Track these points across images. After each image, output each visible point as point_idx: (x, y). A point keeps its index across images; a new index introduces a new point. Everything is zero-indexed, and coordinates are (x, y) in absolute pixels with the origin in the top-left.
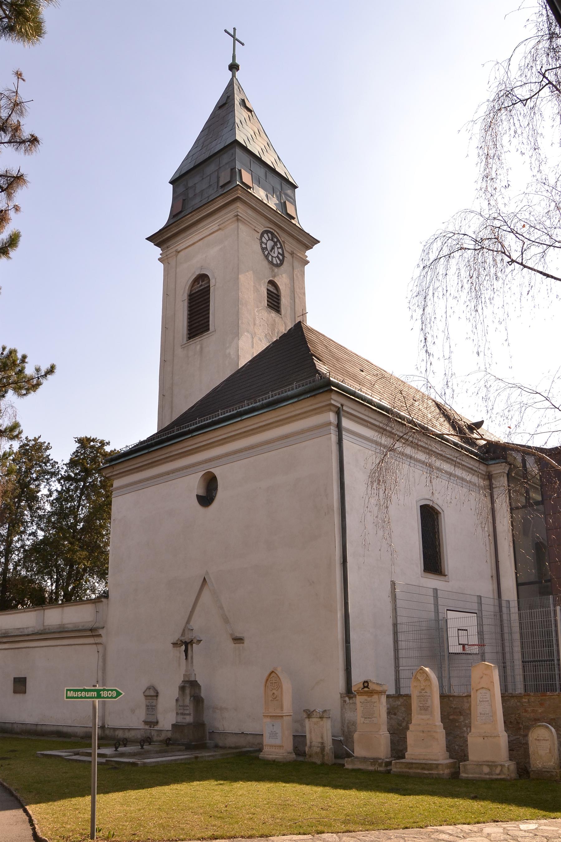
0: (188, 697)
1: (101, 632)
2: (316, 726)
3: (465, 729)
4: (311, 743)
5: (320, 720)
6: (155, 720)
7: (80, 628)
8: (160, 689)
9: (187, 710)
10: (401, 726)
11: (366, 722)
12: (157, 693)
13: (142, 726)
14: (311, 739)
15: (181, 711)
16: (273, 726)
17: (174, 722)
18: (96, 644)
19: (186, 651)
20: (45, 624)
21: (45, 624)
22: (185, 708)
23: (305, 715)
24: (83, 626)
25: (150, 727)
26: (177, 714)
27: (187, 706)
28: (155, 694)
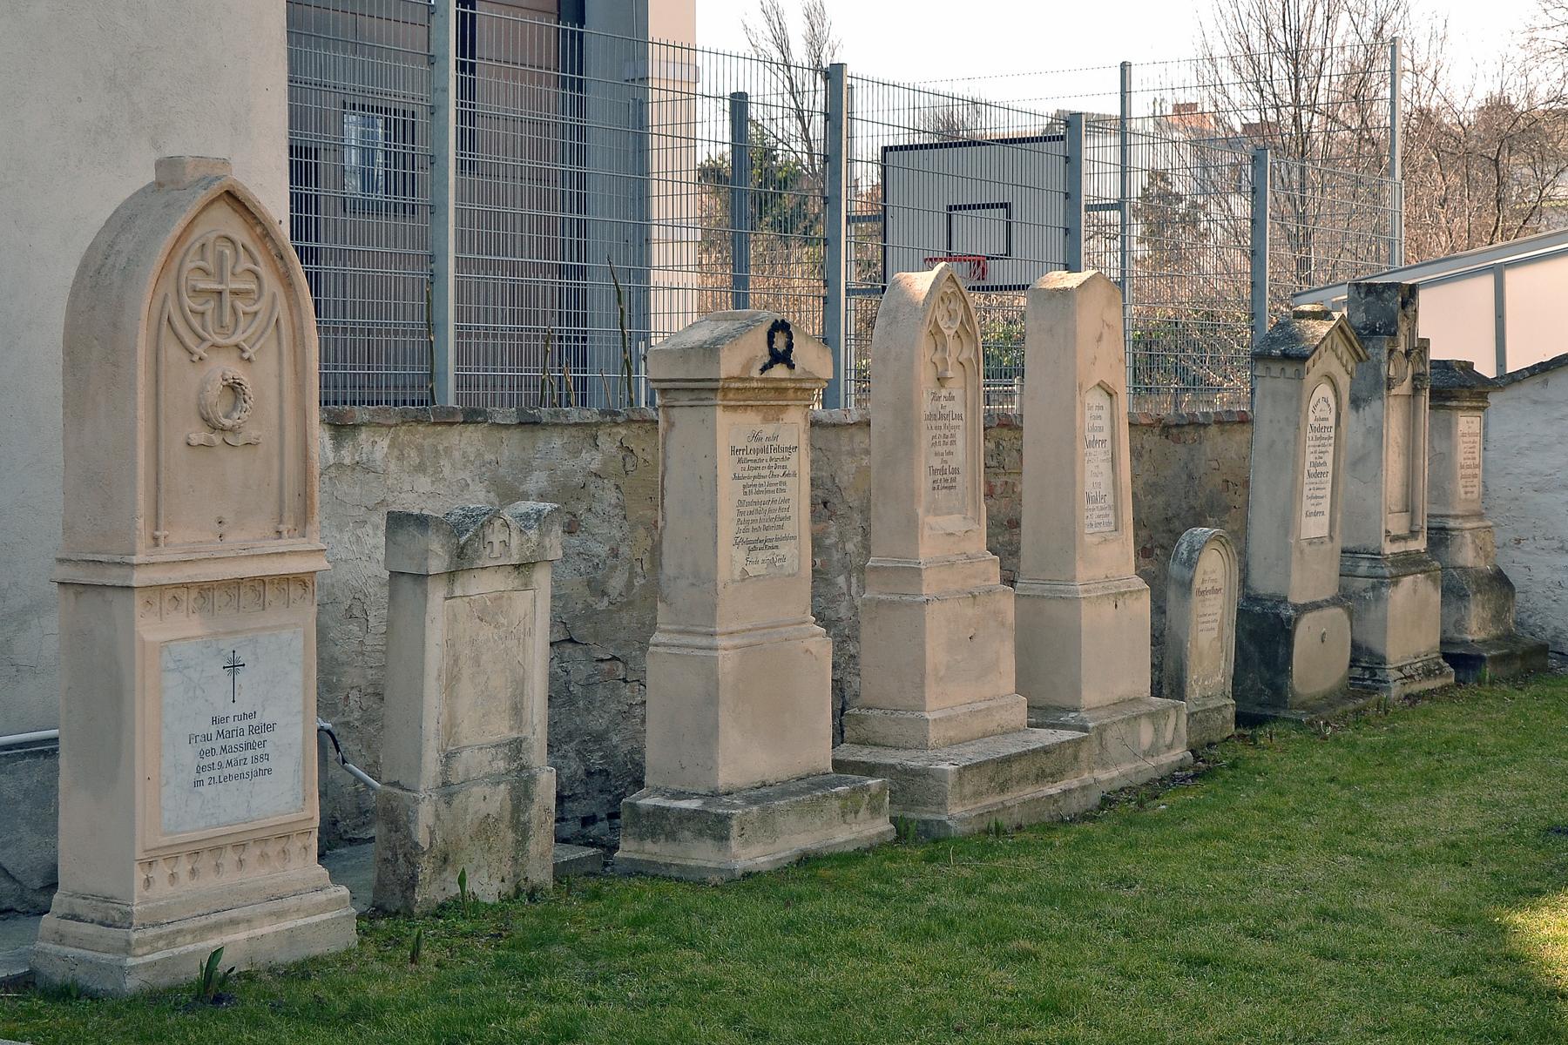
2: (487, 632)
3: (841, 580)
4: (449, 757)
5: (513, 581)
10: (604, 593)
11: (752, 570)
14: (450, 727)
16: (234, 666)
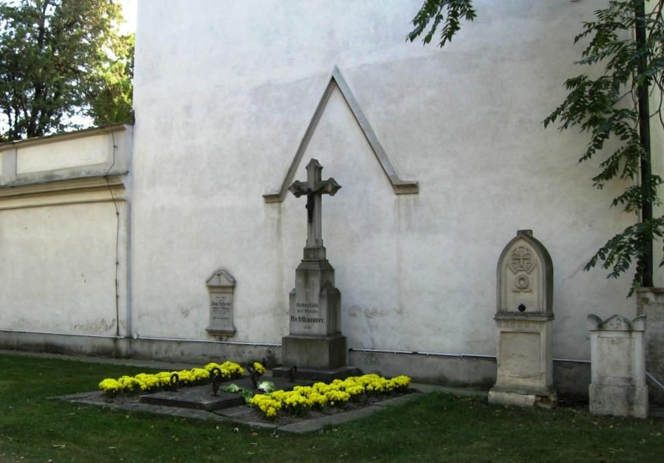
0: (317, 290)
1: (123, 180)
6: (231, 329)
7: (83, 174)
8: (240, 274)
9: (314, 312)
12: (235, 282)
13: (204, 338)
15: (301, 315)
17: (287, 334)
18: (114, 200)
19: (311, 207)
20: (19, 172)
21: (19, 172)
22: (310, 309)
23: (593, 325)
24: (89, 173)
25: (221, 339)
26: (293, 319)
27: (315, 305)
28: (230, 284)
